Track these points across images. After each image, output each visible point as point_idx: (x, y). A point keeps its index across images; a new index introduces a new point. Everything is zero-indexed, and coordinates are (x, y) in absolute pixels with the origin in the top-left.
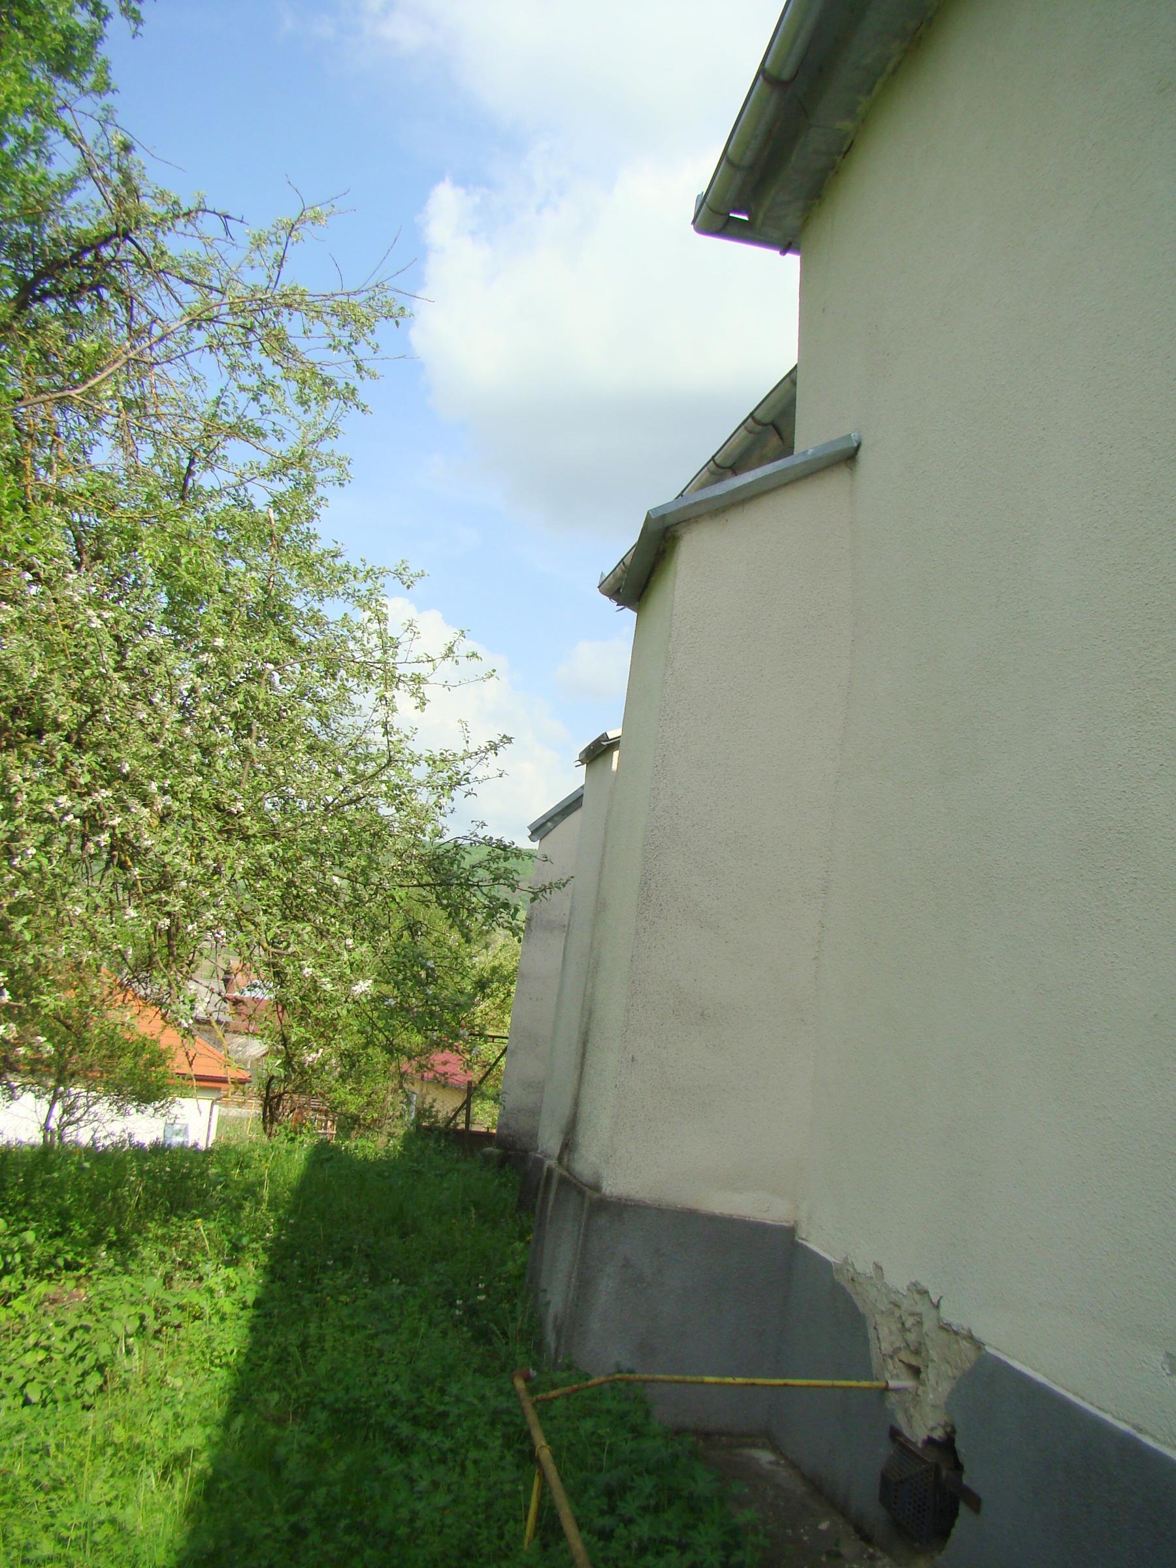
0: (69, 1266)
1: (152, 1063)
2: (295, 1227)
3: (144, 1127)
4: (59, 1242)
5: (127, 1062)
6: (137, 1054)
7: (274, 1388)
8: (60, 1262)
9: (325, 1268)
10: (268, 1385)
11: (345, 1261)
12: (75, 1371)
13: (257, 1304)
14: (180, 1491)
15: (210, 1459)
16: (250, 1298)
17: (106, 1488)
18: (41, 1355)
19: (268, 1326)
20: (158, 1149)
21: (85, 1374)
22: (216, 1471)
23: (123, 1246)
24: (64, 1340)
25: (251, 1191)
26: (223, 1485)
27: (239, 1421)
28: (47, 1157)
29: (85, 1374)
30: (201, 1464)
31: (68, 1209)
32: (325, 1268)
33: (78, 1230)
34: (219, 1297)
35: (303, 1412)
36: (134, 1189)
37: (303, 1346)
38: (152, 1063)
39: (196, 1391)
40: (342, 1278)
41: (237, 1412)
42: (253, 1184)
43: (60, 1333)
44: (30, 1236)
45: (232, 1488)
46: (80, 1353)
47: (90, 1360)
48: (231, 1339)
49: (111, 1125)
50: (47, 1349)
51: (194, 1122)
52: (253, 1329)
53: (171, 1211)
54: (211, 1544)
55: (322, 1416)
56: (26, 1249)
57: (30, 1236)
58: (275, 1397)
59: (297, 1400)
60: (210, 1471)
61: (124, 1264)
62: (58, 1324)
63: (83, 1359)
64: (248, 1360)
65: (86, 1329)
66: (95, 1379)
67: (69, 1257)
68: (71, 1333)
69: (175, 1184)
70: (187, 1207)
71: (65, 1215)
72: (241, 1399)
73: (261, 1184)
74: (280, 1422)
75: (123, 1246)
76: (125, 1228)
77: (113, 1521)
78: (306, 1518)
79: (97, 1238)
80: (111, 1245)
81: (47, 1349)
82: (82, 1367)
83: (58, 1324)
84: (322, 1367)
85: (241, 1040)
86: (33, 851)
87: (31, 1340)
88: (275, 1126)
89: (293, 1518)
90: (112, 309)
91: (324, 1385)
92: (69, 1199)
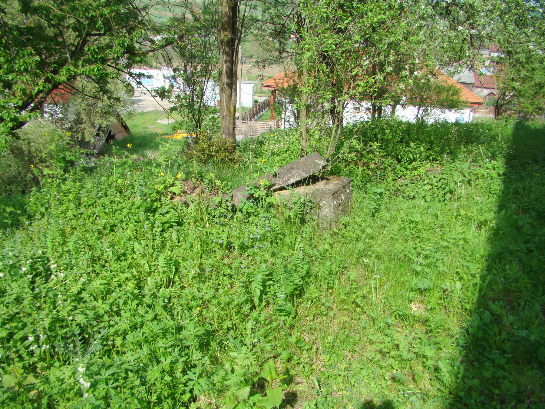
0: (433, 160)
1: (453, 95)
2: (516, 149)
3: (451, 116)
4: (430, 152)
5: (445, 94)
6: (448, 91)
7: (513, 203)
8: (431, 158)
9: (528, 163)
10: (511, 202)
11: (536, 162)
12: (441, 193)
13: (504, 174)
14: (484, 233)
15: (496, 223)
16: (501, 172)
17: (460, 228)
18: (430, 187)
19: (509, 182)
20: (457, 124)
21: (445, 193)
22: (498, 228)
23: (453, 154)
24: (437, 182)
25: (494, 138)
26: (501, 232)
27: (503, 212)
28: (421, 125)
29: (445, 193)
30: (493, 224)
31: (432, 141)
32: (528, 163)
33: (436, 148)
34: (493, 169)
35: (526, 211)
36: (454, 133)
37: (524, 189)
38: (453, 95)
39: (485, 202)
40: (536, 167)
41: (502, 210)
42: (494, 136)
43: (435, 180)
44: (422, 149)
45: (504, 234)
46: (443, 187)
47: (447, 189)
48: (497, 185)
49: (437, 116)
50: (431, 185)
51: (465, 116)
52: (504, 182)
53: (467, 143)
54: (499, 251)
55: (533, 213)
56: (420, 153)
57: (422, 149)
58: (514, 206)
59: (523, 208)
60: (496, 227)
61: (453, 160)
62: (435, 177)
63: (444, 188)
64: (503, 193)
65: (445, 179)
66: (448, 196)
67: (434, 157)
68: (440, 180)
69: (468, 135)
70: (472, 142)
71: (431, 143)
72: (501, 206)
73: (498, 136)
74: (517, 214)
75: (453, 154)
76: (452, 148)
77: (464, 239)
78: (532, 246)
79: (442, 151)
80: (448, 153)
81: (431, 185)
82: (444, 191)
83: (435, 177)
84: (532, 196)
85: (479, 90)
86: (423, 7)
87: (426, 182)
88: (500, 117)
89: (528, 246)
90: (78, 327)
91: (534, 203)
92: (432, 138)
